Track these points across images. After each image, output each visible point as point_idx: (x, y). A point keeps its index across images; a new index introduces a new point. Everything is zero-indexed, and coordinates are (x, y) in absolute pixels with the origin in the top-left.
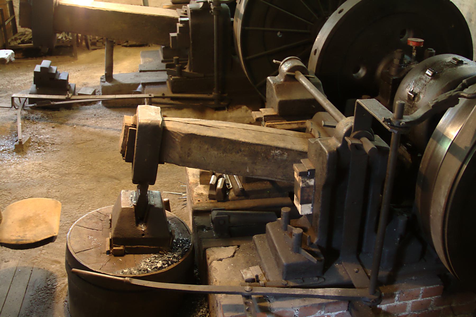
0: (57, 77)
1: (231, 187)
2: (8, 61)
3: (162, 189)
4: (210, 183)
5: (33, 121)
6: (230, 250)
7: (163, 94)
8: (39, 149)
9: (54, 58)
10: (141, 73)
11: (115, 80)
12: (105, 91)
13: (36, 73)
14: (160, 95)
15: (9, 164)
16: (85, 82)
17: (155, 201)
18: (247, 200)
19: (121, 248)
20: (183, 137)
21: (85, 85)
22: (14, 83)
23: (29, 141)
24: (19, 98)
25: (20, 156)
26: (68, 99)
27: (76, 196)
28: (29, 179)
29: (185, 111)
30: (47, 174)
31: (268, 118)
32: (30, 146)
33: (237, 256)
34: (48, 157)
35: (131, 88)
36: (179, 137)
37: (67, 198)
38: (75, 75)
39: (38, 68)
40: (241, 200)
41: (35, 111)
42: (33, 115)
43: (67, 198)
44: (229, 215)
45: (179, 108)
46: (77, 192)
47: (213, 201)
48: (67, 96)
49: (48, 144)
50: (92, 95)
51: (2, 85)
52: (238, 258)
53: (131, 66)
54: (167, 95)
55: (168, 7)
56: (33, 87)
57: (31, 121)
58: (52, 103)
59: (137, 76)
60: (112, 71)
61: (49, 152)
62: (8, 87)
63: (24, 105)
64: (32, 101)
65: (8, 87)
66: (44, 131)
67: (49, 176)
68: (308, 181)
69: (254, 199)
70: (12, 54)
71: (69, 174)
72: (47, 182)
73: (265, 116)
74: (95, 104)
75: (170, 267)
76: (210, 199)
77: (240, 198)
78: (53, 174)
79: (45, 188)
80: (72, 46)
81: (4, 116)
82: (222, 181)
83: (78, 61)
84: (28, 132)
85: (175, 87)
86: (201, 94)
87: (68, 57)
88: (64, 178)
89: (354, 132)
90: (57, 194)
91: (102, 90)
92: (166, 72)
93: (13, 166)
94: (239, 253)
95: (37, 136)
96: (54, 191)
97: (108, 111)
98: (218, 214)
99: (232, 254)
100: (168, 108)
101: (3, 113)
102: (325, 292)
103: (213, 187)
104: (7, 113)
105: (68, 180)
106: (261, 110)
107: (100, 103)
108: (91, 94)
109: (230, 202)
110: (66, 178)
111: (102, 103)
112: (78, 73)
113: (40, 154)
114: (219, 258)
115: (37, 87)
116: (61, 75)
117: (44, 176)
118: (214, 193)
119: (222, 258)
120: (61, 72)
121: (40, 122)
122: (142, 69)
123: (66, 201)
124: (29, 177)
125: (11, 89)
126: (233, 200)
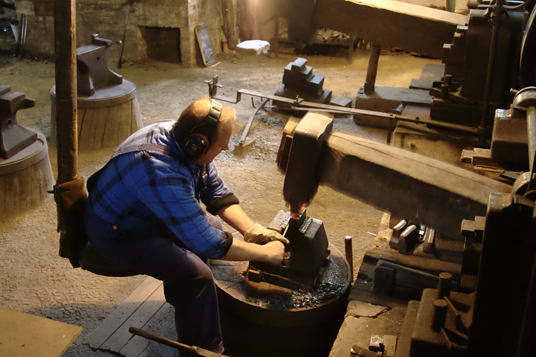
0: (308, 80)
1: (424, 240)
2: (259, 53)
3: (368, 228)
4: (395, 228)
5: (269, 124)
6: (376, 310)
7: (418, 118)
8: (259, 156)
9: (309, 58)
10: (412, 90)
11: (376, 94)
12: (360, 104)
13: (286, 71)
14: (414, 118)
15: (220, 164)
16: (348, 91)
17: (309, 231)
18: (436, 260)
19: (258, 272)
20: (343, 158)
21: (346, 94)
22: (270, 80)
23: (251, 145)
24: (262, 97)
25: (236, 159)
26: (297, 105)
27: (270, 214)
28: (231, 184)
29: (439, 143)
30: (252, 183)
31: (478, 161)
32: (251, 151)
33: (380, 318)
34: (264, 167)
35: (389, 105)
36: (339, 156)
37: (259, 214)
38: (341, 81)
39: (289, 67)
40: (428, 257)
41: (276, 114)
42: (271, 118)
43: (259, 214)
44: (395, 271)
45: (432, 138)
46: (274, 210)
47: (393, 251)
48: (295, 101)
49: (271, 152)
50: (346, 106)
51: (256, 80)
52: (379, 320)
53: (404, 78)
54: (422, 119)
55: (461, 11)
56: (281, 87)
57: (267, 124)
58: (293, 108)
59: (404, 93)
60: (374, 82)
61: (269, 161)
62: (262, 83)
63: (264, 104)
64: (275, 102)
65: (262, 83)
66: (274, 137)
67: (254, 186)
68: (474, 245)
69: (447, 261)
70: (267, 46)
71: (275, 188)
72: (248, 192)
73: (474, 157)
74: (346, 117)
75: (301, 309)
76: (391, 248)
77: (429, 255)
78: (259, 185)
79: (243, 198)
80: (347, 48)
81: (243, 113)
82: (413, 228)
83: (351, 66)
84: (257, 135)
85: (436, 111)
86: (463, 125)
87: (344, 60)
88: (268, 191)
89: (529, 190)
90: (252, 207)
91: (356, 102)
92: (429, 92)
93: (223, 168)
94: (384, 315)
95: (264, 141)
96: (250, 202)
97: (357, 128)
98: (382, 265)
99: (375, 314)
100: (419, 135)
101: (242, 111)
102: (130, 290)
103: (397, 233)
104: (247, 111)
105: (271, 195)
106: (475, 149)
107: (352, 118)
108: (344, 105)
109: (414, 257)
110: (271, 192)
111: (354, 118)
112: (344, 80)
113: (258, 161)
114: (357, 314)
115: (285, 87)
116: (315, 78)
117: (248, 186)
118: (396, 241)
119: (360, 315)
120: (315, 75)
121: (276, 127)
122: (414, 85)
123: (257, 216)
124: (233, 183)
125: (263, 85)
126: (419, 255)
